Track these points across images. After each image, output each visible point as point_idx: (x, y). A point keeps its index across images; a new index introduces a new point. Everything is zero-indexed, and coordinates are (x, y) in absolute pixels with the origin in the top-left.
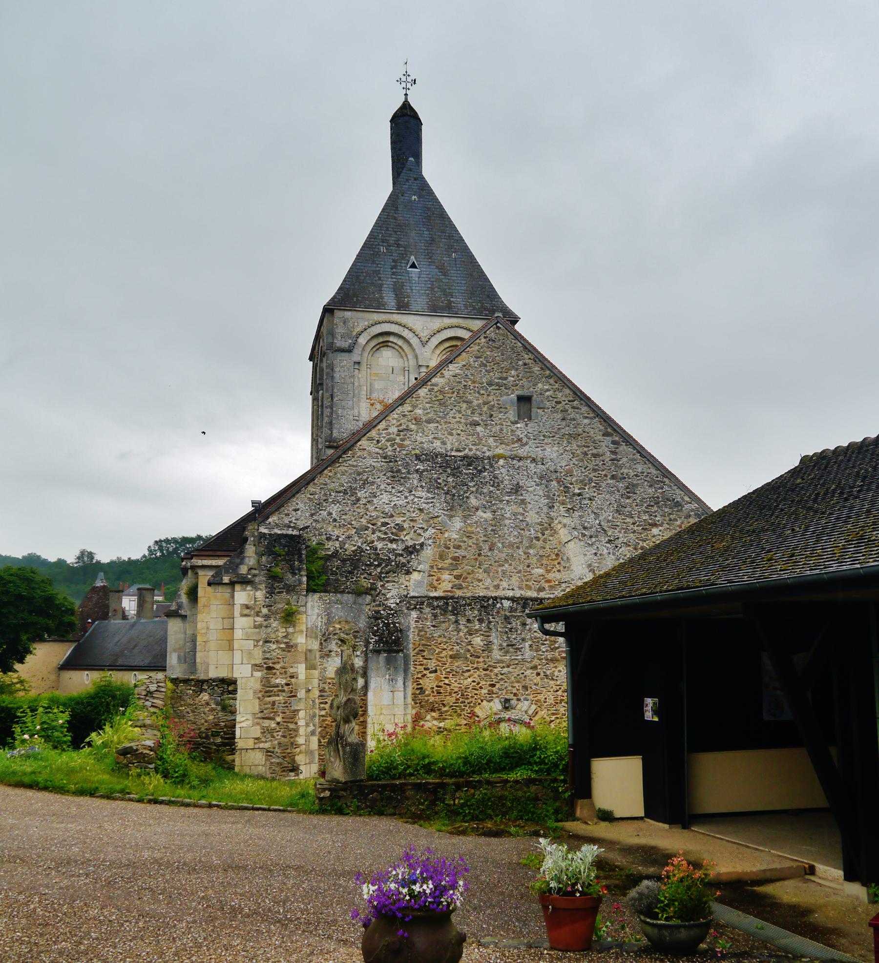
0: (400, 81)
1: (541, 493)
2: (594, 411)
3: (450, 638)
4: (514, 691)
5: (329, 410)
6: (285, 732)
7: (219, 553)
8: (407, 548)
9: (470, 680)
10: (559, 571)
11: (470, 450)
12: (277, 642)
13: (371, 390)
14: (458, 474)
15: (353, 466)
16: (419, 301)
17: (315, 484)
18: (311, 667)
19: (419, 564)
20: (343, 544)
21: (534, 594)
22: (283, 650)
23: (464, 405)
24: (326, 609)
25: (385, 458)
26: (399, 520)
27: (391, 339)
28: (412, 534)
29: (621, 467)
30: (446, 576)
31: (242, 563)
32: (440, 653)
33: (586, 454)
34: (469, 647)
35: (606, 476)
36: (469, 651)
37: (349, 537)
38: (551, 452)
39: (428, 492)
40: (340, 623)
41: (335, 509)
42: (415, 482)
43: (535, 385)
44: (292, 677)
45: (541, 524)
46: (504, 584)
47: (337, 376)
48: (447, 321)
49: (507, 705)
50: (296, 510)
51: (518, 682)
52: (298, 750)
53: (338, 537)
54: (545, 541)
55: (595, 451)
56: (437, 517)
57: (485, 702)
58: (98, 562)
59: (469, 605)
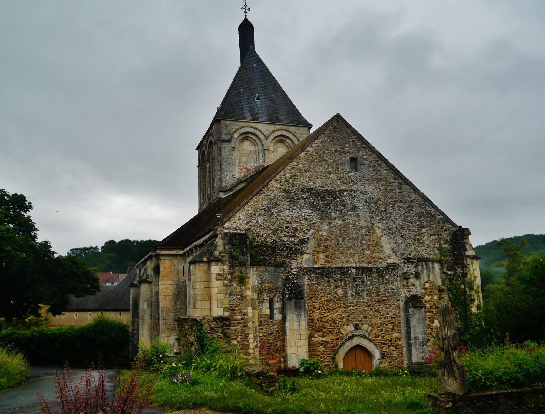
0: (242, 8)
1: (367, 210)
2: (389, 166)
3: (326, 291)
4: (360, 319)
5: (219, 172)
6: (242, 347)
7: (179, 247)
8: (300, 241)
9: (337, 314)
10: (378, 252)
11: (328, 187)
12: (236, 294)
13: (240, 162)
14: (324, 200)
15: (268, 195)
16: (263, 117)
17: (248, 205)
18: (254, 309)
19: (307, 249)
20: (265, 239)
21: (366, 265)
22: (239, 299)
23: (324, 163)
24: (260, 275)
25: (285, 190)
26: (295, 225)
27: (250, 136)
28: (302, 233)
29: (404, 196)
30: (321, 256)
31: (215, 249)
32: (321, 299)
33: (386, 189)
34: (336, 295)
35: (397, 201)
36: (336, 297)
37: (269, 235)
38: (369, 188)
39: (309, 209)
40: (268, 283)
41: (260, 219)
42: (302, 204)
43: (359, 152)
44: (245, 315)
45: (367, 227)
46: (351, 260)
47: (223, 154)
48: (278, 127)
49: (357, 327)
50: (239, 220)
51: (361, 314)
52: (250, 357)
53: (263, 235)
54: (370, 236)
55: (390, 188)
56: (315, 223)
57: (345, 326)
58: (60, 258)
59: (335, 272)
